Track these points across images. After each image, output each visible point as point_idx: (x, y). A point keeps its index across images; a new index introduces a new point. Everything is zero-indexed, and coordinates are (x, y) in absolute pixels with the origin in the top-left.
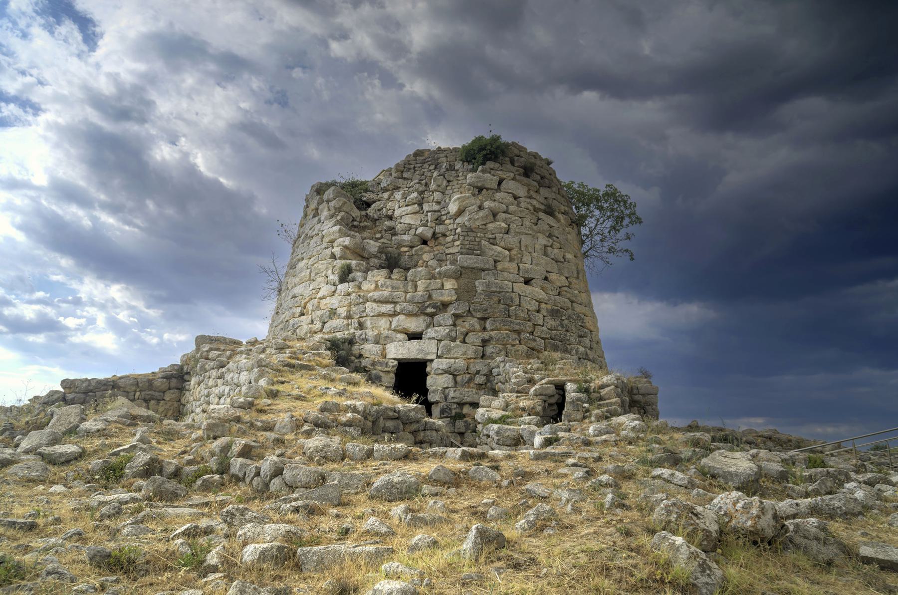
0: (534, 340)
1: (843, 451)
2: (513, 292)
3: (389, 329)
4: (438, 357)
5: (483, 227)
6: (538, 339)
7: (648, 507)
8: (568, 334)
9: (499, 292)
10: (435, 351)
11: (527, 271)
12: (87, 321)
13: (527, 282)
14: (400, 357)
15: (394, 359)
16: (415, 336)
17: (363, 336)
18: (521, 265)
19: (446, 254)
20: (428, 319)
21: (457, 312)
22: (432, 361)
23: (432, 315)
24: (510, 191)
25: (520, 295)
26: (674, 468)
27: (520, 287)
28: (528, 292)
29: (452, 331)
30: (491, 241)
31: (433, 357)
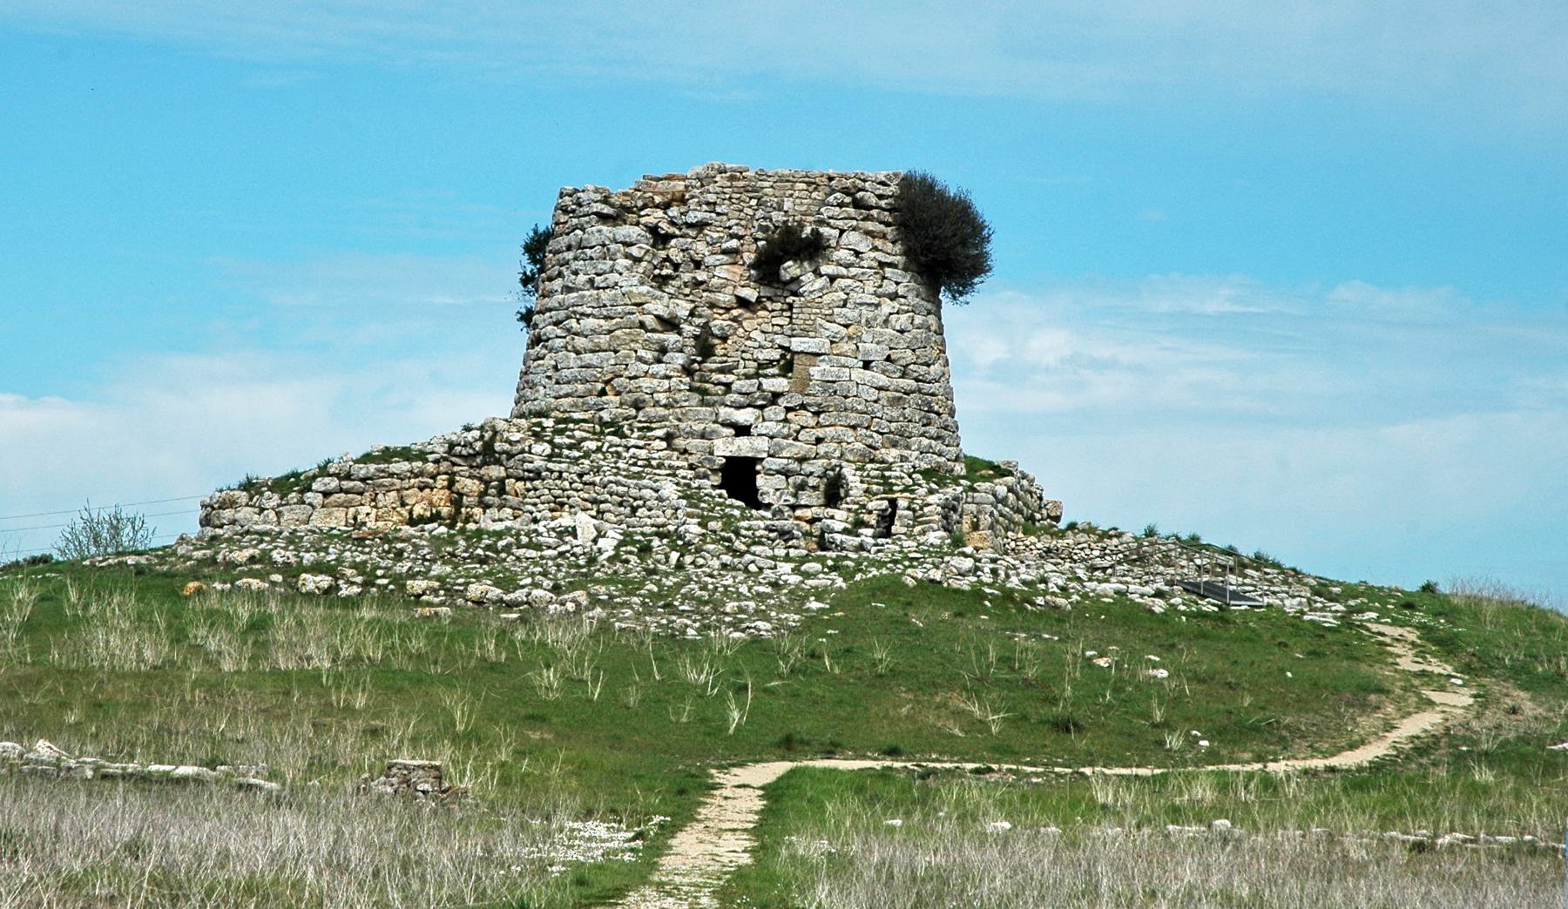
0: (872, 437)
1: (460, 465)
2: (850, 380)
3: (715, 422)
4: (770, 456)
5: (819, 300)
6: (875, 435)
7: (893, 555)
8: (911, 425)
9: (834, 382)
10: (767, 449)
11: (867, 353)
12: (482, 446)
13: (867, 365)
14: (729, 454)
15: (724, 457)
16: (742, 430)
17: (688, 429)
18: (860, 345)
19: (773, 325)
20: (757, 412)
21: (789, 405)
22: (763, 459)
23: (762, 407)
24: (850, 247)
25: (857, 384)
26: (1443, 659)
27: (858, 374)
28: (867, 379)
29: (784, 427)
30: (828, 318)
31: (765, 455)
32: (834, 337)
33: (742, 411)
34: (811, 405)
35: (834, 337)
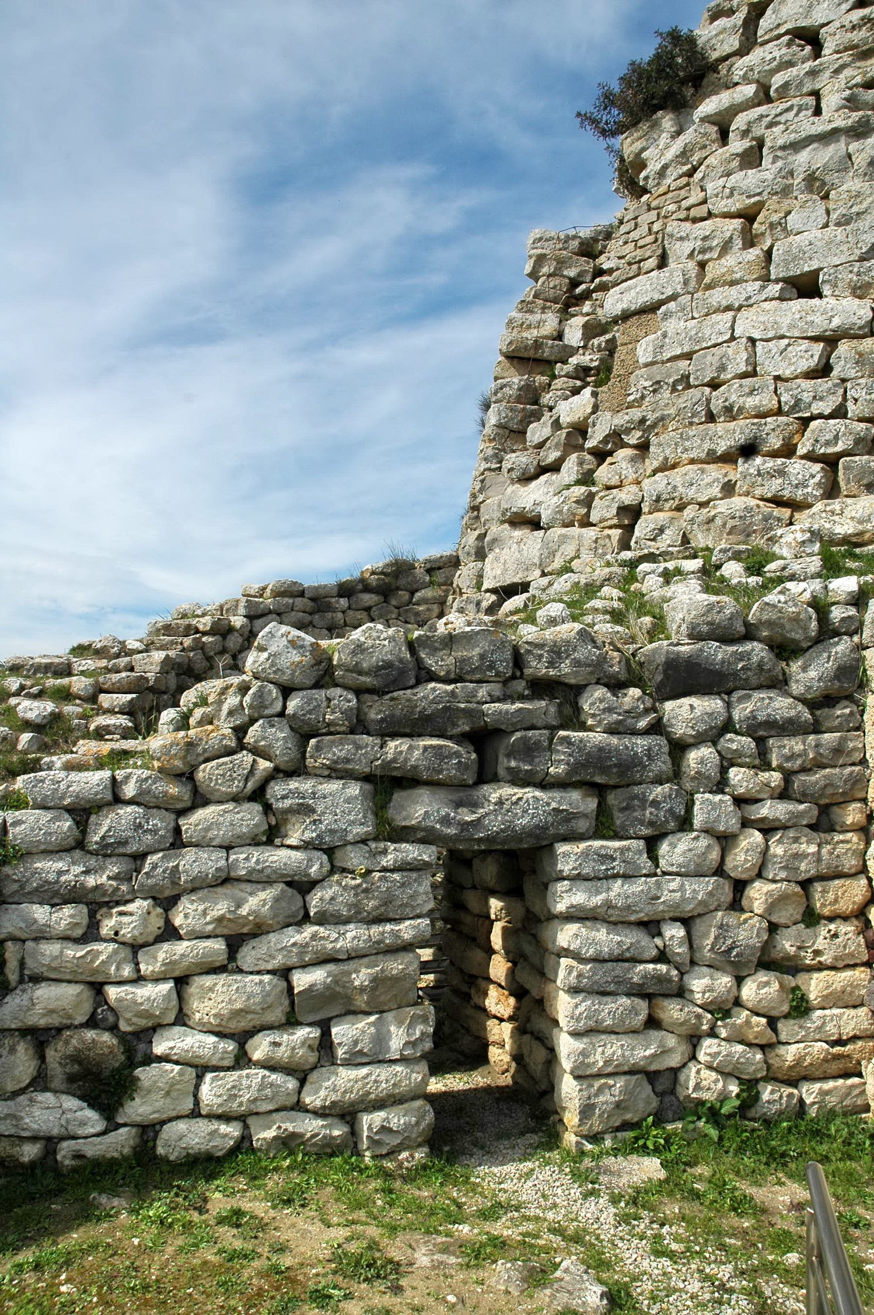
32: (703, 251)
33: (534, 483)
34: (628, 431)
35: (703, 251)
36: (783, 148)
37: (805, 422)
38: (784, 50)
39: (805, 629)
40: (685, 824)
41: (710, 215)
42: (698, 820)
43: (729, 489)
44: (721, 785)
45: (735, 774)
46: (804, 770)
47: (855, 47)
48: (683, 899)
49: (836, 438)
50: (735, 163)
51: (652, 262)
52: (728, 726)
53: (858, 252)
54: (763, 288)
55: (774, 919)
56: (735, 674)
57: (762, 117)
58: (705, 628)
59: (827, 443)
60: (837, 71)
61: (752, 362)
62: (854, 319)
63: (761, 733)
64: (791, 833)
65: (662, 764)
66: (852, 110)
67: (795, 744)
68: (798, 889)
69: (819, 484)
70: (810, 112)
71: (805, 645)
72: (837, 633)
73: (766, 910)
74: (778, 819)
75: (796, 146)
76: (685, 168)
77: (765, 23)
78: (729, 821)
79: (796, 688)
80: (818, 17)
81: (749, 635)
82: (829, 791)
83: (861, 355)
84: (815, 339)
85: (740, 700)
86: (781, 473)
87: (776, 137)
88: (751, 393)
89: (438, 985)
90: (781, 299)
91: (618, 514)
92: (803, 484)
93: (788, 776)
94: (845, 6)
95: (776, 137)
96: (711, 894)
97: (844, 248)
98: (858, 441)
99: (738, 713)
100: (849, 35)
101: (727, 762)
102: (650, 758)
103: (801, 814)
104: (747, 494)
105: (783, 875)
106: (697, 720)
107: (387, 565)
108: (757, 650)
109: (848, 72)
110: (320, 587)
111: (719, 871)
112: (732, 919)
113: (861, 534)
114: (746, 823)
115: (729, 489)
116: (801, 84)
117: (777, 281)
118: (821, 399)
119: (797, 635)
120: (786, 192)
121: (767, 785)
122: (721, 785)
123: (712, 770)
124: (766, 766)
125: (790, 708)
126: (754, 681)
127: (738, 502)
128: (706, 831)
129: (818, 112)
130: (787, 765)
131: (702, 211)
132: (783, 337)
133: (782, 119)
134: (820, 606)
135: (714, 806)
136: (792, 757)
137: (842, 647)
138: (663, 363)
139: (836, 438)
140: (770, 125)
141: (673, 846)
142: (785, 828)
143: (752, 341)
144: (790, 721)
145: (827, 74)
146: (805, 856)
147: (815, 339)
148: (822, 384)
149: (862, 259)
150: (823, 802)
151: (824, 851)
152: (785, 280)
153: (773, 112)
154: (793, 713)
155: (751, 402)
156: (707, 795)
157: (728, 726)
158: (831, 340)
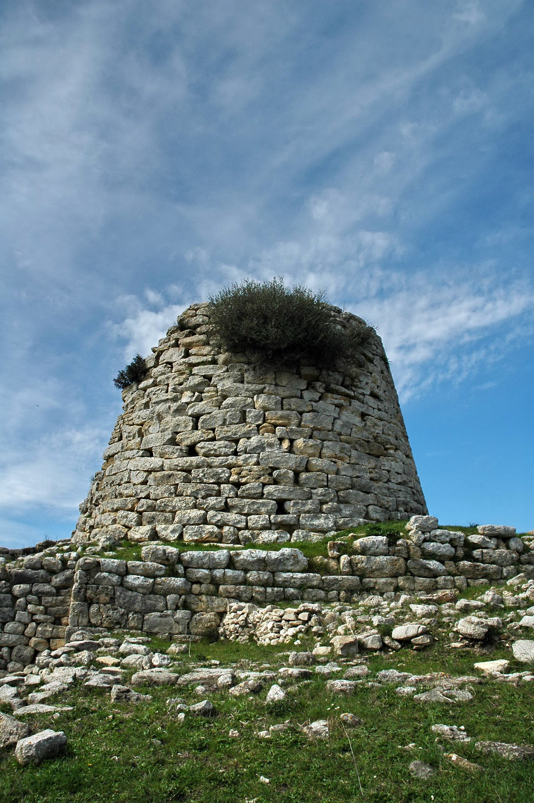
36: (154, 403)
37: (139, 499)
38: (163, 369)
39: (57, 567)
40: (13, 619)
41: (133, 424)
42: (17, 617)
43: (114, 521)
44: (25, 609)
45: (30, 607)
46: (51, 606)
47: (180, 371)
48: (8, 640)
49: (143, 505)
50: (143, 407)
51: (117, 439)
52: (30, 592)
53: (163, 442)
54: (138, 452)
55: (37, 649)
56: (34, 578)
57: (152, 391)
58: (28, 565)
59: (140, 507)
60: (174, 378)
61: (129, 478)
62: (156, 465)
63: (40, 595)
64: (45, 624)
65: (8, 602)
66: (174, 392)
67: (50, 599)
68: (45, 640)
69: (135, 521)
70: (164, 391)
71: (58, 571)
72: (68, 569)
73: (34, 646)
74: (40, 620)
75: (157, 403)
76: (133, 406)
77: (161, 358)
78: (27, 620)
79: (53, 583)
80: (173, 359)
81: (42, 568)
82: (58, 613)
83: (155, 477)
84: (145, 471)
85: (35, 586)
86: (126, 517)
87: (154, 399)
88: (126, 489)
89: (116, 760)
90: (142, 456)
91: (89, 528)
92: (131, 521)
93: (46, 608)
94: (180, 357)
95: (154, 399)
96: (17, 639)
97: (160, 440)
98: (148, 507)
99: (35, 589)
100: (179, 367)
101: (28, 603)
102: (5, 600)
103: (48, 619)
104: (119, 523)
105: (40, 636)
106: (20, 590)
107: (44, 543)
108: (42, 572)
109: (177, 379)
110: (15, 550)
111: (23, 634)
112: (23, 648)
113: (141, 538)
114: (33, 621)
115: (114, 521)
116: (164, 381)
117: (142, 450)
118: (143, 492)
119: (55, 569)
120: (152, 418)
121: (39, 610)
122: (25, 609)
123: (23, 605)
124: (40, 604)
125: (49, 588)
126: (41, 581)
127: (117, 526)
128: (20, 622)
129: (167, 392)
130: (46, 605)
131: (131, 423)
132: (139, 470)
133: (157, 393)
134: (64, 561)
135: (21, 615)
136: (48, 602)
137: (68, 573)
138: (112, 475)
139: (143, 505)
140: (154, 394)
141: (8, 625)
142: (44, 623)
143: (131, 470)
144: (48, 592)
145: (171, 379)
146: (48, 631)
147: (145, 471)
148: (144, 487)
149: (164, 445)
150: (57, 616)
151: (54, 630)
152: (145, 450)
153: (155, 390)
154: (50, 590)
155: (126, 492)
156: (21, 612)
157: (30, 592)
158: (149, 472)
